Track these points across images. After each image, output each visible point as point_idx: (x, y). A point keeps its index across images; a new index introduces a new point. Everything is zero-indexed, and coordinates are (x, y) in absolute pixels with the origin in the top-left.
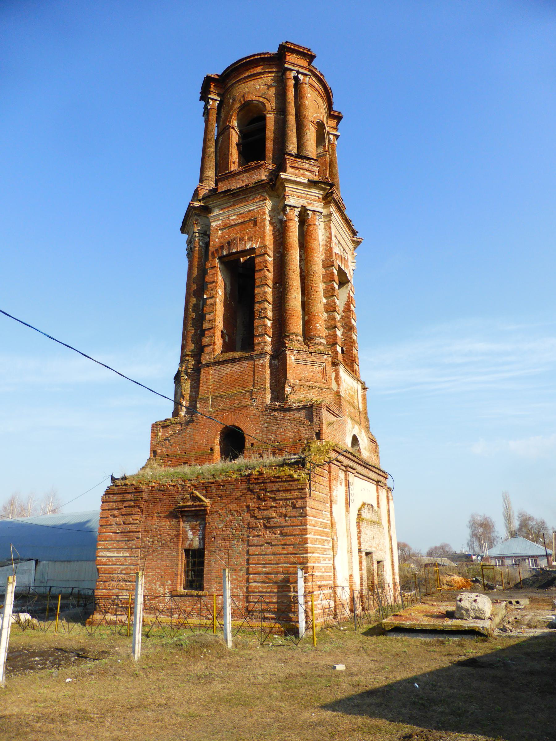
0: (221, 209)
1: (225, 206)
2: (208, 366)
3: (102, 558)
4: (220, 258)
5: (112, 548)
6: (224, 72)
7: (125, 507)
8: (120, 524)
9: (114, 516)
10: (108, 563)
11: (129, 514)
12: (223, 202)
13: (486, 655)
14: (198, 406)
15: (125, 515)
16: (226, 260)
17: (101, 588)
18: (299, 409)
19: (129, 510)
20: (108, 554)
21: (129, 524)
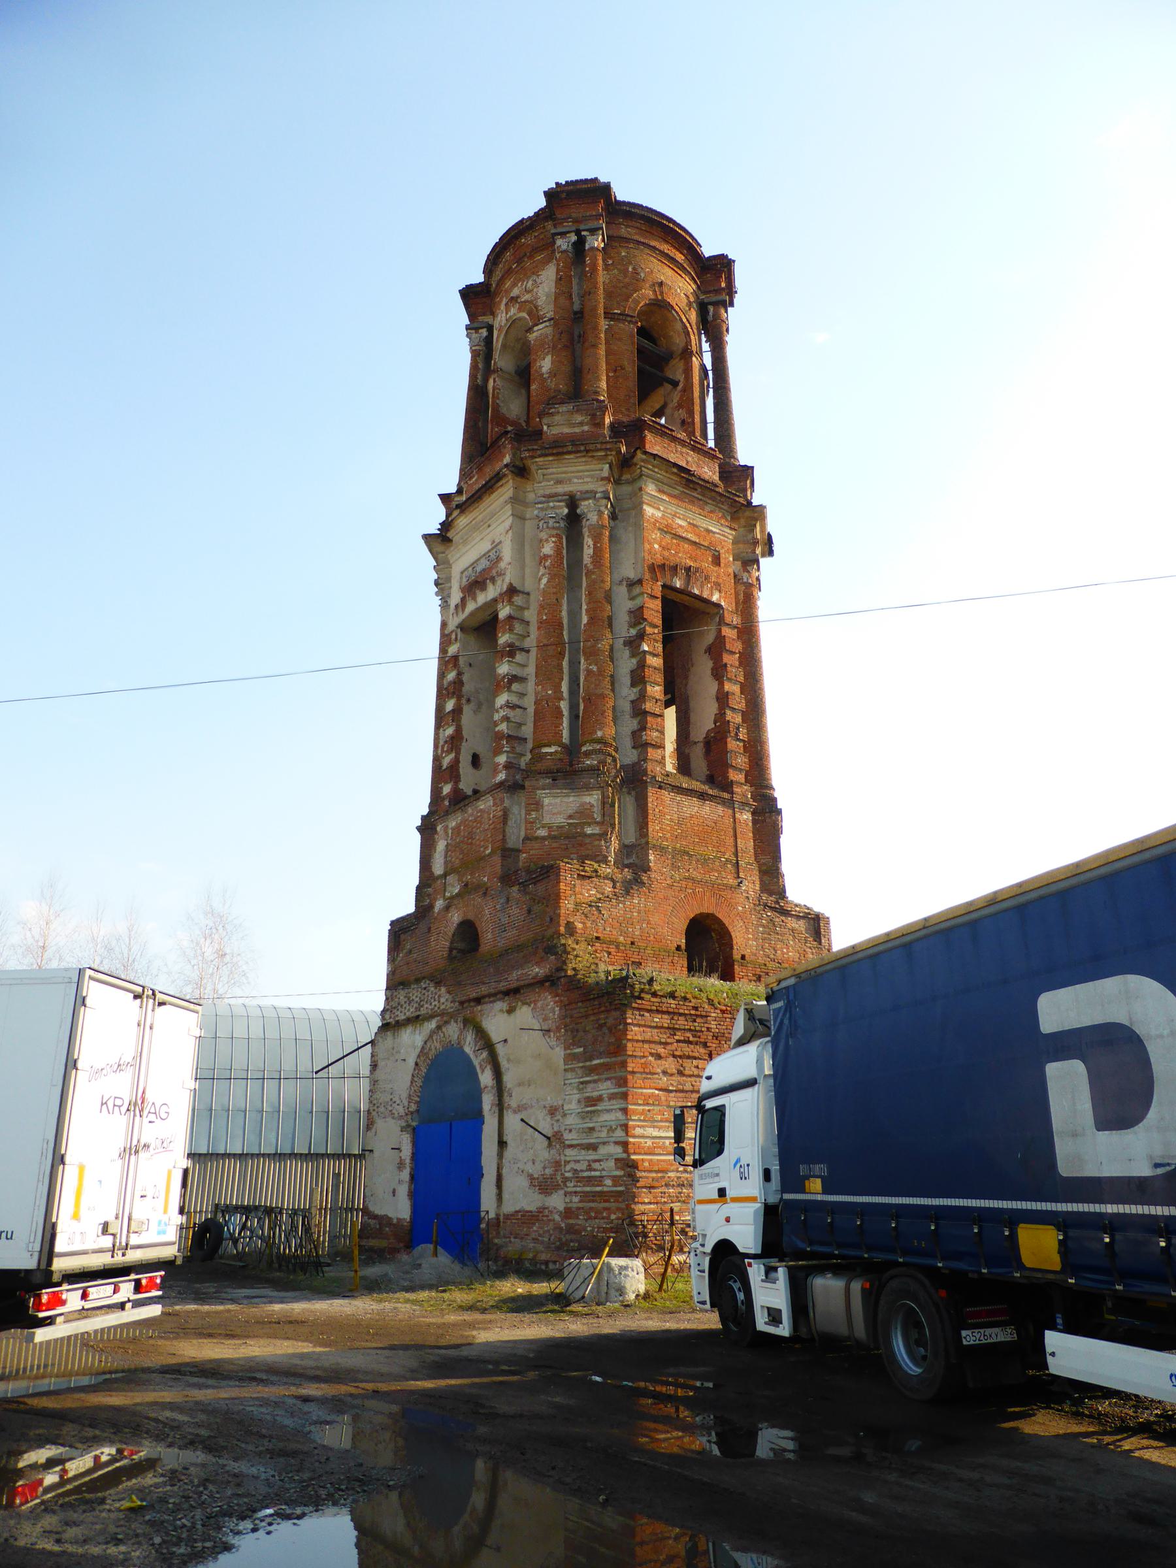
0: (660, 491)
1: (666, 488)
2: (660, 787)
3: (642, 1140)
4: (664, 586)
5: (661, 1121)
6: (624, 202)
7: (678, 1041)
8: (672, 1075)
9: (659, 1057)
10: (657, 1151)
11: (689, 1057)
12: (665, 480)
13: (239, 1359)
14: (651, 858)
15: (680, 1057)
16: (672, 596)
17: (646, 1200)
18: (798, 917)
19: (687, 1049)
20: (656, 1133)
21: (690, 1076)
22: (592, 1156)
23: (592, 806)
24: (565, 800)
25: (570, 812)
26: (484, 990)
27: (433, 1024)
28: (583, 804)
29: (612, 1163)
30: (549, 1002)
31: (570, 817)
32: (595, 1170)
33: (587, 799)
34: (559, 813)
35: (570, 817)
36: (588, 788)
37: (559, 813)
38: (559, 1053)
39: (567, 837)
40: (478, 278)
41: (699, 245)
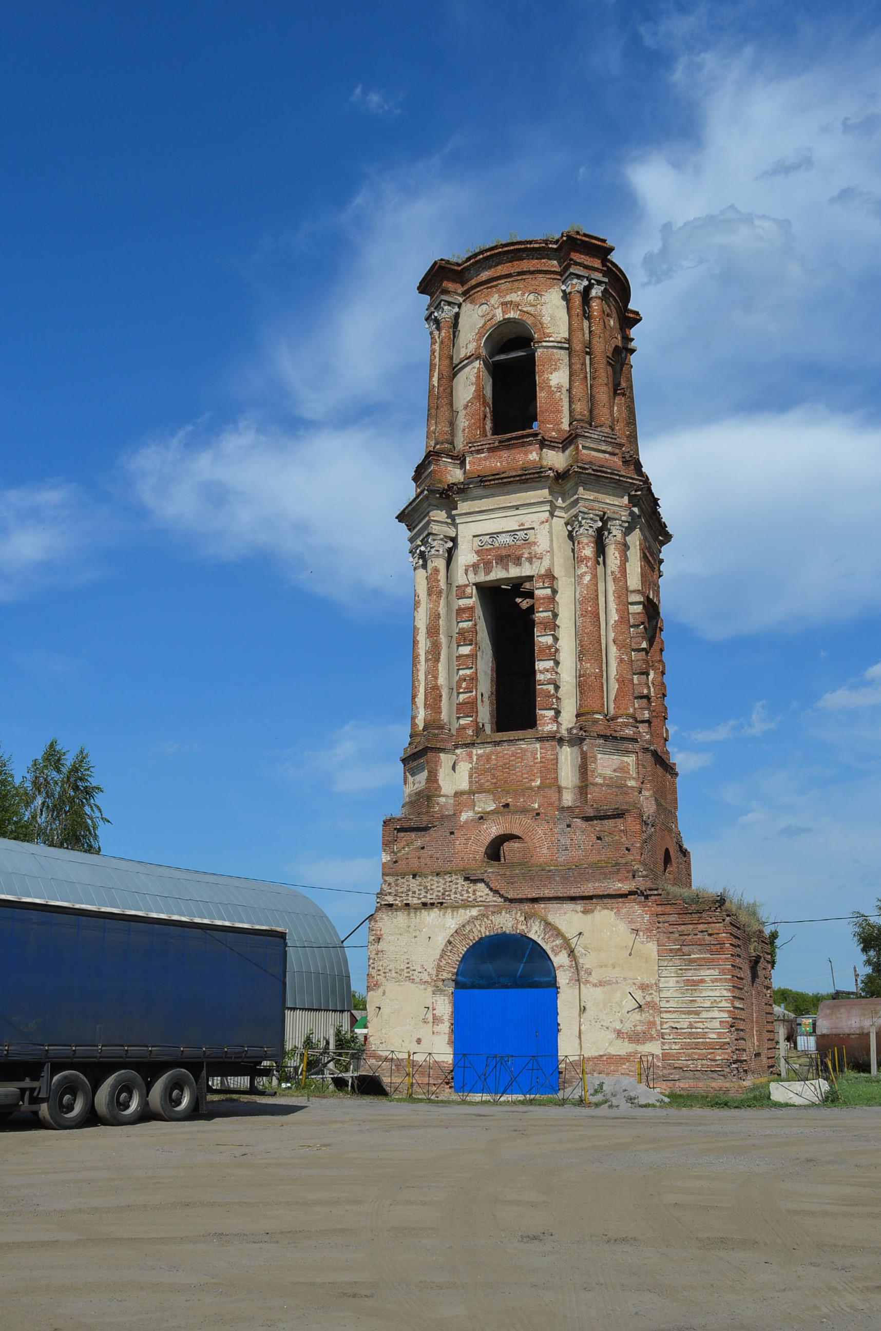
22: (692, 1018)
23: (629, 764)
24: (612, 757)
25: (614, 767)
26: (547, 893)
27: (474, 912)
28: (623, 762)
29: (716, 1024)
30: (638, 912)
31: (615, 771)
32: (262, 1093)
33: (626, 759)
34: (607, 767)
35: (615, 771)
36: (627, 752)
37: (607, 767)
38: (652, 948)
39: (617, 787)
40: (634, 332)
41: (604, 241)
